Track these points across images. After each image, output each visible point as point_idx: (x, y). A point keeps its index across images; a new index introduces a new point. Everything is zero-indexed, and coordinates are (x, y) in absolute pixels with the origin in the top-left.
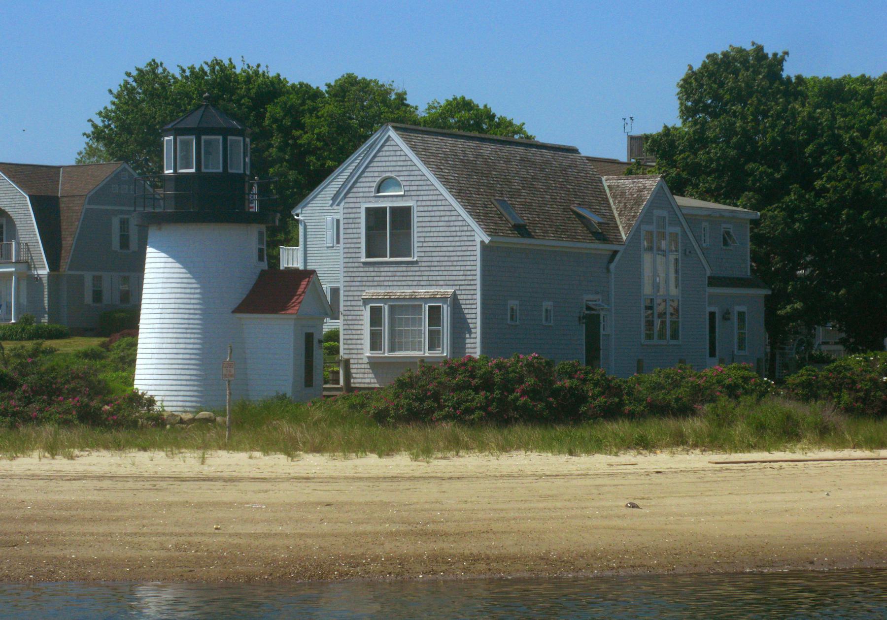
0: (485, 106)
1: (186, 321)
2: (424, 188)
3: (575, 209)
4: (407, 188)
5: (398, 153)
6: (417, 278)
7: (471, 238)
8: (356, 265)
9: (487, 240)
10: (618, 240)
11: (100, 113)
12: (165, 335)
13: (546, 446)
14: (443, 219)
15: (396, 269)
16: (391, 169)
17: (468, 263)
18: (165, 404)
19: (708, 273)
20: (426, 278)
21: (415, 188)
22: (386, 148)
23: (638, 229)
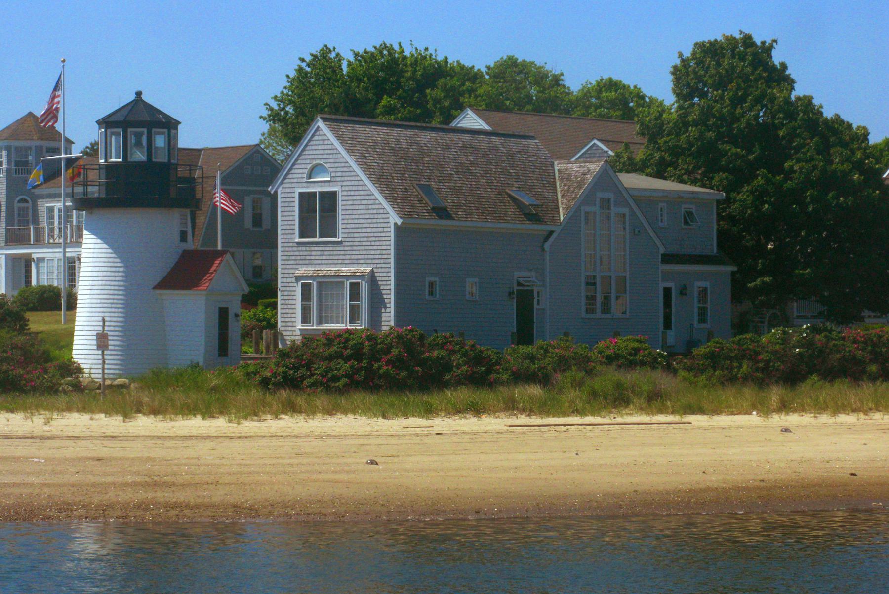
0: (635, 87)
1: (111, 297)
2: (347, 174)
3: (513, 194)
4: (333, 174)
5: (326, 142)
6: (341, 257)
7: (386, 220)
8: (291, 245)
9: (399, 222)
10: (554, 220)
11: (275, 98)
12: (94, 310)
13: (368, 411)
14: (363, 202)
15: (323, 249)
16: (320, 156)
17: (384, 243)
18: (93, 371)
19: (662, 250)
20: (348, 257)
21: (339, 174)
22: (316, 138)
23: (578, 210)
